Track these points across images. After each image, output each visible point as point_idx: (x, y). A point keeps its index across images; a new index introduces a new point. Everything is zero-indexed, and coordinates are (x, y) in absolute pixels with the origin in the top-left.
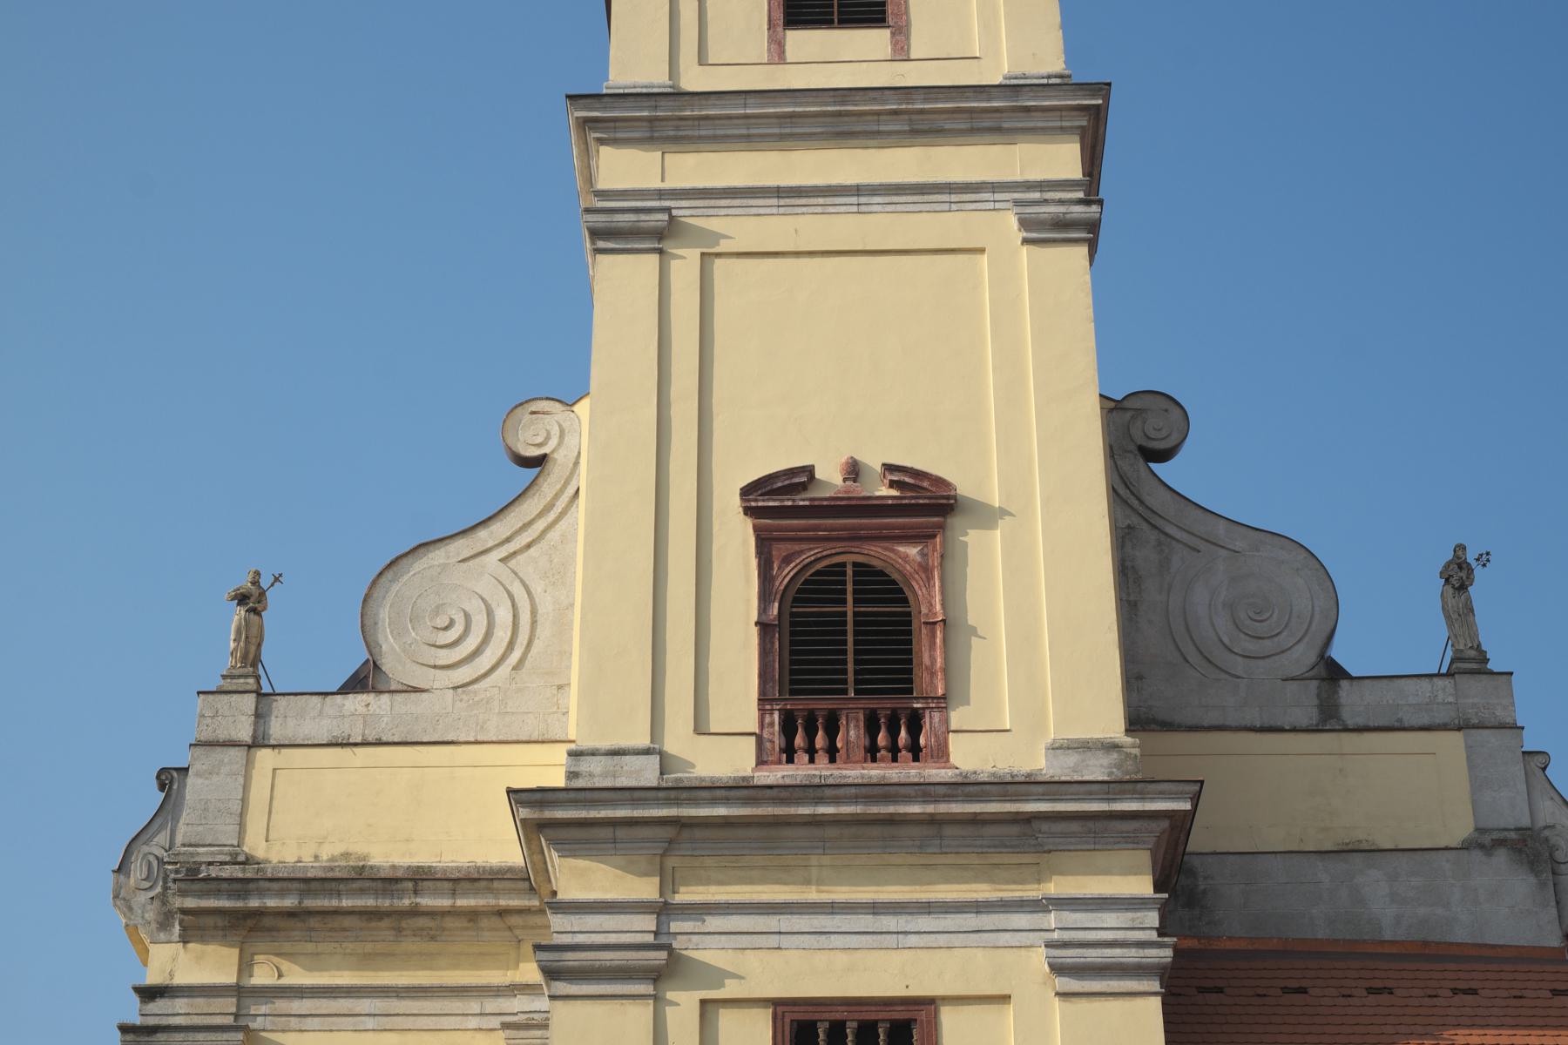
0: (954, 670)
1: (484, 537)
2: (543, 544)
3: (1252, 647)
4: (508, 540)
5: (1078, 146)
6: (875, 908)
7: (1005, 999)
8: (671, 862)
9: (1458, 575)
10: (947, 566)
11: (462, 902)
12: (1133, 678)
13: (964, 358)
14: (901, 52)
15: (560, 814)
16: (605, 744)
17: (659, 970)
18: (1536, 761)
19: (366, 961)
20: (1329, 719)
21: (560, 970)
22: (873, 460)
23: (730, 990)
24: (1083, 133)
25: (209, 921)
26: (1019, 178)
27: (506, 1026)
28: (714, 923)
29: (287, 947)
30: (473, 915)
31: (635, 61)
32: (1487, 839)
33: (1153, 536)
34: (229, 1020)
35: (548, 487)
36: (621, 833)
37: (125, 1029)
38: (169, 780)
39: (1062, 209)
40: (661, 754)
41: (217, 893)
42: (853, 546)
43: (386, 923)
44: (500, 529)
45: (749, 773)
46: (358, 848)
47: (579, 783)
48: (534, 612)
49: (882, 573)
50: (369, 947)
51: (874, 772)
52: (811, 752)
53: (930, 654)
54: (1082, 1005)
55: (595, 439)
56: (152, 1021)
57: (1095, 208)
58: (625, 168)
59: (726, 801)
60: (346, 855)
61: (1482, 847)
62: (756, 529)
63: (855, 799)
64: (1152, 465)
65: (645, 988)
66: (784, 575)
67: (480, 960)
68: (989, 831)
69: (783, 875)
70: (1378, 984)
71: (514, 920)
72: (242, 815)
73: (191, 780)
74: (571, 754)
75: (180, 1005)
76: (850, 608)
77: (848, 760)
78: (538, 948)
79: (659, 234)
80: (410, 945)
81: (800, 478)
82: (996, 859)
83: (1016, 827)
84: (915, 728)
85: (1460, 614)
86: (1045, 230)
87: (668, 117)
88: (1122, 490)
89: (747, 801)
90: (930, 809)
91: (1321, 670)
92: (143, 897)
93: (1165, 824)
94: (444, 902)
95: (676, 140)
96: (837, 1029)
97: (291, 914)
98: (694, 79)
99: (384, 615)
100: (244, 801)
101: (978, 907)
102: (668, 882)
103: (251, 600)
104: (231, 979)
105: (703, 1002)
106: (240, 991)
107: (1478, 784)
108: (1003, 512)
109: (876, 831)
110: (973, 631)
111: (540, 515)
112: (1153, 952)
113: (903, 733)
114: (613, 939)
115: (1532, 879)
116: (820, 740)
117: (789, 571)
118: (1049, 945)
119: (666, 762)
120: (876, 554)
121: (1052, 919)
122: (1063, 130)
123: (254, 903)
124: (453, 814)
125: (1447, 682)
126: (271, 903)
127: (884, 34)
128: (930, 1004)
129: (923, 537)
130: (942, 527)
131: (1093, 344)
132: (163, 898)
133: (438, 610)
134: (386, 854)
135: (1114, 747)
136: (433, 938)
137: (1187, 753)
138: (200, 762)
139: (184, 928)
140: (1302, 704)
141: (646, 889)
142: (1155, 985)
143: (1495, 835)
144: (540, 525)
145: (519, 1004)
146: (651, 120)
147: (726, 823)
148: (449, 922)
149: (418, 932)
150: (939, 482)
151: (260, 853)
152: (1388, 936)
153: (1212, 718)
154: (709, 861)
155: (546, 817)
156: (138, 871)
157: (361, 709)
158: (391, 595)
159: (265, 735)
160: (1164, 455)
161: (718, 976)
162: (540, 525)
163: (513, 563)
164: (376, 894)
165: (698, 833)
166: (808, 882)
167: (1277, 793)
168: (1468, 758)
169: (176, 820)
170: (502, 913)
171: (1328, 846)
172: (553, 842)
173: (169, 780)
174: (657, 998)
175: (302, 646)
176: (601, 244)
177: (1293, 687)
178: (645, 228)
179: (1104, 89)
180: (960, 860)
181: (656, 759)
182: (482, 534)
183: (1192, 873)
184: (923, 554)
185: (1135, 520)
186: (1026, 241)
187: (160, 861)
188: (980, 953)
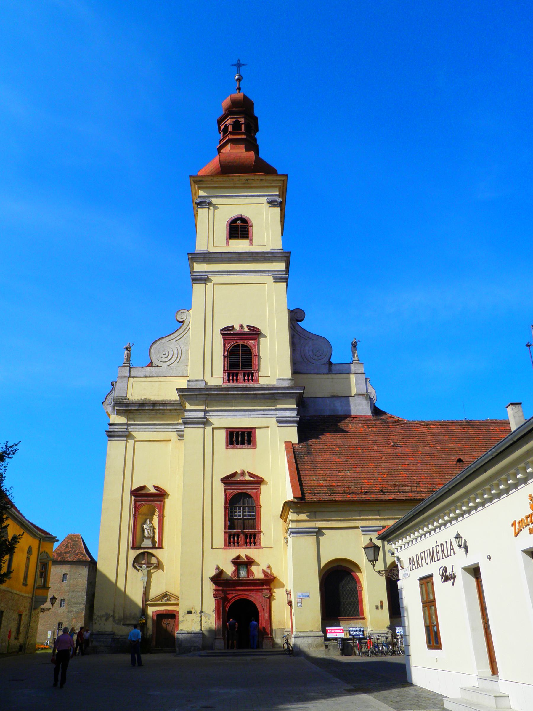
3: (317, 358)
5: (284, 264)
7: (268, 427)
12: (294, 363)
13: (261, 304)
14: (251, 244)
17: (206, 423)
20: (330, 372)
24: (285, 261)
25: (121, 411)
27: (177, 431)
30: (170, 410)
31: (201, 246)
35: (184, 327)
36: (198, 396)
42: (241, 341)
43: (154, 411)
47: (190, 387)
51: (245, 385)
52: (233, 380)
53: (255, 361)
55: (194, 317)
57: (287, 276)
58: (198, 267)
66: (228, 346)
74: (188, 381)
75: (116, 427)
76: (240, 353)
78: (182, 418)
80: (159, 415)
83: (271, 396)
84: (252, 376)
86: (277, 280)
87: (208, 257)
93: (297, 395)
95: (208, 261)
98: (212, 250)
101: (264, 410)
106: (127, 425)
117: (229, 346)
118: (277, 417)
119: (206, 383)
120: (245, 342)
121: (277, 412)
122: (282, 260)
124: (165, 390)
127: (249, 240)
129: (254, 339)
133: (163, 351)
136: (163, 414)
137: (304, 379)
138: (119, 380)
142: (296, 425)
145: (179, 427)
147: (217, 395)
148: (166, 411)
149: (160, 413)
155: (186, 394)
160: (300, 321)
165: (212, 397)
167: (320, 386)
170: (176, 410)
174: (204, 428)
182: (172, 336)
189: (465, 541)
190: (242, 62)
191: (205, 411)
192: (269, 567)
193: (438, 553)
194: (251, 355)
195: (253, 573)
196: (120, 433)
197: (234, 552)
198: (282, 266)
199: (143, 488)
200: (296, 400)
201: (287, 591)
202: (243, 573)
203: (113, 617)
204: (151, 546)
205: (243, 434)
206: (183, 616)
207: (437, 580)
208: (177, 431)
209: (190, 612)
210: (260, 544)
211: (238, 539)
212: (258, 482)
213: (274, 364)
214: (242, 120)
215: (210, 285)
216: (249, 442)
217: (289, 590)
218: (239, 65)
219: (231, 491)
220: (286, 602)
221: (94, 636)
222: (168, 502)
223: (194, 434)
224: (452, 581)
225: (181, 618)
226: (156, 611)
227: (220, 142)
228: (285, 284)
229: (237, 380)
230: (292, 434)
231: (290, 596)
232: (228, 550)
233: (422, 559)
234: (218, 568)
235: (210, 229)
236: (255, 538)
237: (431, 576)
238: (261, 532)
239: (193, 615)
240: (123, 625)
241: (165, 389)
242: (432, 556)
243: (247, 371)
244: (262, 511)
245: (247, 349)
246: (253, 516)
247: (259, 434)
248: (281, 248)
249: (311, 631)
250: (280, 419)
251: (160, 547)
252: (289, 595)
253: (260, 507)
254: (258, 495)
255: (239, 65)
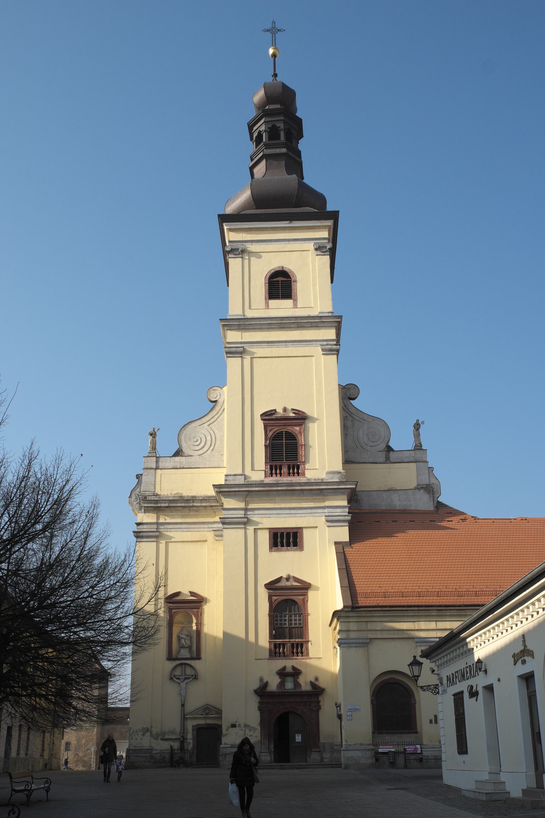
0: (306, 456)
1: (204, 420)
2: (217, 422)
3: (372, 444)
4: (209, 420)
6: (290, 509)
7: (316, 527)
8: (247, 499)
9: (417, 426)
10: (305, 432)
11: (203, 504)
14: (295, 306)
15: (224, 490)
16: (233, 473)
17: (246, 522)
18: (431, 469)
19: (183, 516)
20: (387, 460)
21: (225, 522)
22: (289, 407)
23: (260, 526)
25: (150, 509)
26: (321, 338)
27: (213, 531)
28: (256, 512)
29: (166, 514)
30: (205, 507)
31: (235, 310)
32: (419, 487)
33: (351, 418)
34: (155, 530)
35: (217, 408)
36: (237, 493)
37: (134, 532)
38: (139, 477)
39: (331, 347)
40: (245, 475)
41: (151, 503)
43: (187, 509)
44: (207, 418)
45: (263, 479)
46: (180, 492)
47: (228, 483)
48: (215, 437)
49: (291, 433)
50: (184, 514)
52: (276, 474)
53: (301, 452)
54: (332, 528)
55: (227, 396)
56: (139, 530)
57: (338, 346)
58: (233, 336)
59: (258, 487)
60: (178, 493)
61: (418, 489)
62: (264, 424)
63: (285, 486)
64: (351, 401)
65: (243, 526)
66: (270, 434)
67: (208, 516)
68: (313, 492)
69: (271, 501)
70: (394, 520)
71: (214, 508)
72: (155, 484)
73: (143, 477)
75: (145, 526)
77: (284, 476)
79: (241, 353)
80: (192, 513)
81: (273, 412)
82: (315, 497)
83: (319, 491)
85: (417, 435)
86: (327, 351)
87: (243, 324)
88: (344, 408)
89: (263, 487)
90: (301, 488)
91: (386, 449)
92: (135, 503)
93: (350, 490)
94: (199, 504)
95: (244, 329)
96: (282, 534)
97: (167, 507)
98: (249, 314)
99: (183, 438)
100: (155, 481)
102: (247, 504)
103: (153, 435)
104: (155, 521)
105: (255, 529)
106: (157, 524)
107: (418, 475)
108: (317, 419)
109: (290, 492)
110: (310, 446)
111: (216, 415)
112: (347, 517)
113: (296, 470)
114: (235, 516)
115: (428, 496)
116: (278, 471)
117: (271, 433)
119: (246, 477)
120: (289, 429)
121: (326, 510)
122: (331, 326)
123: (159, 505)
125: (413, 452)
126: (163, 505)
127: (291, 301)
128: (301, 528)
129: (300, 425)
130: (304, 423)
131: (337, 379)
132: (139, 503)
133: (194, 437)
134: (187, 493)
135: (340, 473)
138: (145, 473)
139: (145, 510)
140: (381, 457)
141: (242, 505)
142: (347, 524)
143: (421, 486)
144: (216, 417)
145: (216, 525)
146: (238, 325)
148: (200, 508)
149: (193, 510)
150: (303, 413)
151: (159, 493)
152: (398, 508)
153: (363, 460)
154: (255, 499)
155: (223, 490)
156: (134, 497)
157: (179, 460)
158: (184, 434)
159: (158, 466)
160: (354, 399)
161: (257, 523)
162: (216, 417)
163: (210, 426)
164: (185, 503)
165: (253, 493)
166: (276, 503)
168: (417, 469)
169: (141, 485)
170: (211, 506)
171: (386, 489)
172: (222, 495)
173: (139, 477)
175: (166, 447)
176: (228, 355)
177: (380, 453)
178: (237, 351)
179: (340, 317)
180: (308, 498)
181: (243, 476)
182: (203, 419)
183: (357, 495)
184: (300, 429)
185: (347, 415)
186: (323, 354)
187: (138, 495)
188: (311, 518)
189: (485, 665)
190: (278, 26)
191: (246, 510)
192: (317, 679)
193: (467, 673)
194: (296, 444)
195: (301, 685)
196: (150, 534)
197: (280, 663)
198: (330, 334)
199: (178, 594)
200: (348, 497)
201: (336, 704)
202: (289, 685)
203: (151, 732)
204: (189, 656)
205: (288, 534)
206: (227, 730)
207: (466, 695)
208: (213, 531)
209: (234, 726)
210: (308, 654)
211: (284, 648)
212: (305, 587)
213: (323, 454)
214: (281, 125)
215: (247, 360)
216: (295, 544)
217: (339, 703)
218: (274, 30)
219: (276, 598)
220: (335, 715)
221: (131, 751)
222: (207, 609)
223: (234, 535)
224: (475, 698)
225: (224, 732)
226: (197, 725)
227: (252, 160)
228: (336, 356)
229: (281, 474)
230: (343, 534)
231: (340, 709)
232: (273, 661)
233: (456, 678)
234: (261, 680)
235: (245, 291)
236: (302, 648)
237: (462, 692)
238: (308, 641)
239: (237, 728)
240: (162, 739)
241: (199, 481)
242: (463, 676)
243: (292, 463)
244: (310, 619)
245: (292, 438)
246: (300, 624)
247: (307, 535)
248: (331, 310)
249: (361, 744)
250: (330, 518)
251: (198, 658)
252: (338, 708)
253: (308, 615)
254: (305, 602)
255: (274, 30)
